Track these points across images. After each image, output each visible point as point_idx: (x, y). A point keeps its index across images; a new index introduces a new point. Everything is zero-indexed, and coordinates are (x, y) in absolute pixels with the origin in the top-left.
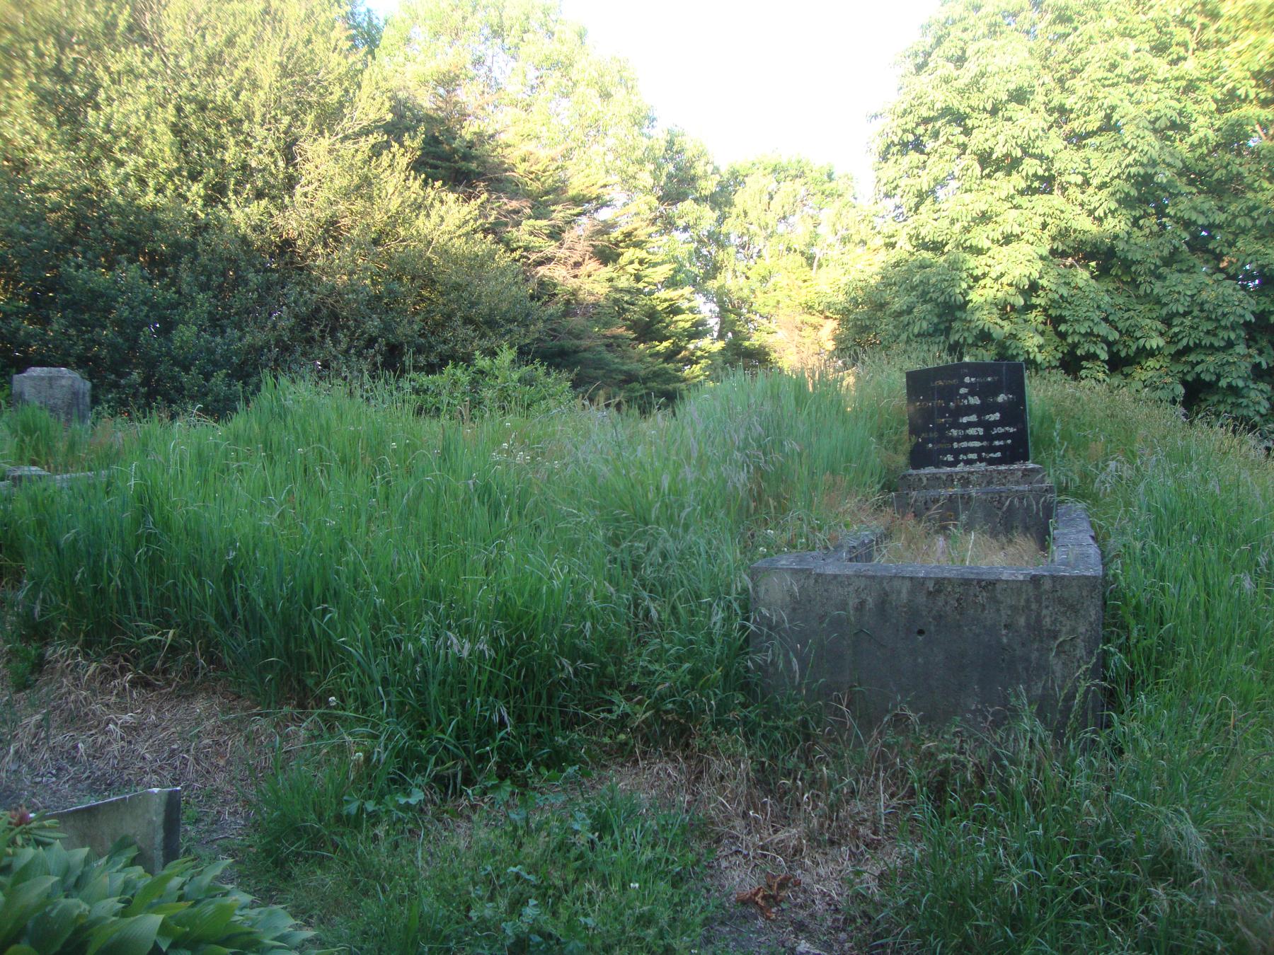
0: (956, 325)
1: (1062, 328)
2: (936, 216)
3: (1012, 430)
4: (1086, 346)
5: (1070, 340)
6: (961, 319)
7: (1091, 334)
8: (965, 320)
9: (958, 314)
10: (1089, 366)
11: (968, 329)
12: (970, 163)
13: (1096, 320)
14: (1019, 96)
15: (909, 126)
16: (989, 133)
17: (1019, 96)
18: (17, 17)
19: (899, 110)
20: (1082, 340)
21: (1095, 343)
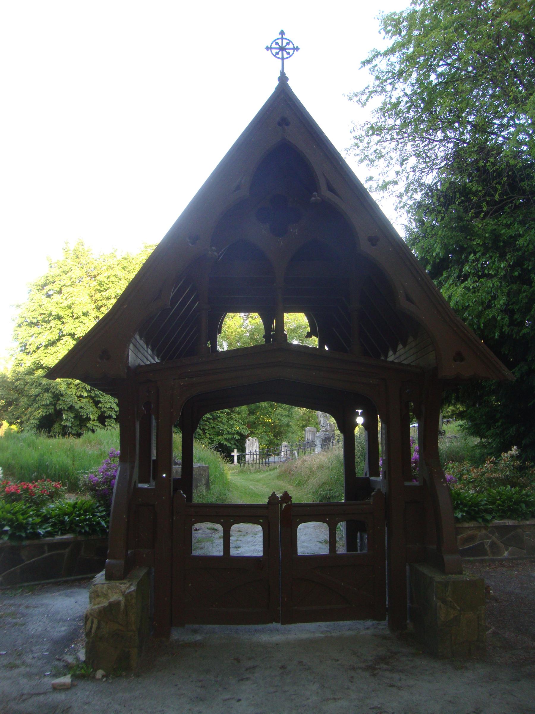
0: (60, 402)
1: (100, 405)
2: (45, 355)
3: (360, 420)
4: (109, 412)
5: (103, 410)
6: (62, 400)
7: (111, 408)
8: (64, 401)
9: (61, 398)
10: (109, 421)
11: (65, 404)
12: (68, 339)
13: (113, 403)
14: (85, 314)
15: (35, 316)
16: (73, 326)
17: (85, 314)
18: (505, 523)
19: (32, 309)
20: (107, 410)
21: (112, 411)
